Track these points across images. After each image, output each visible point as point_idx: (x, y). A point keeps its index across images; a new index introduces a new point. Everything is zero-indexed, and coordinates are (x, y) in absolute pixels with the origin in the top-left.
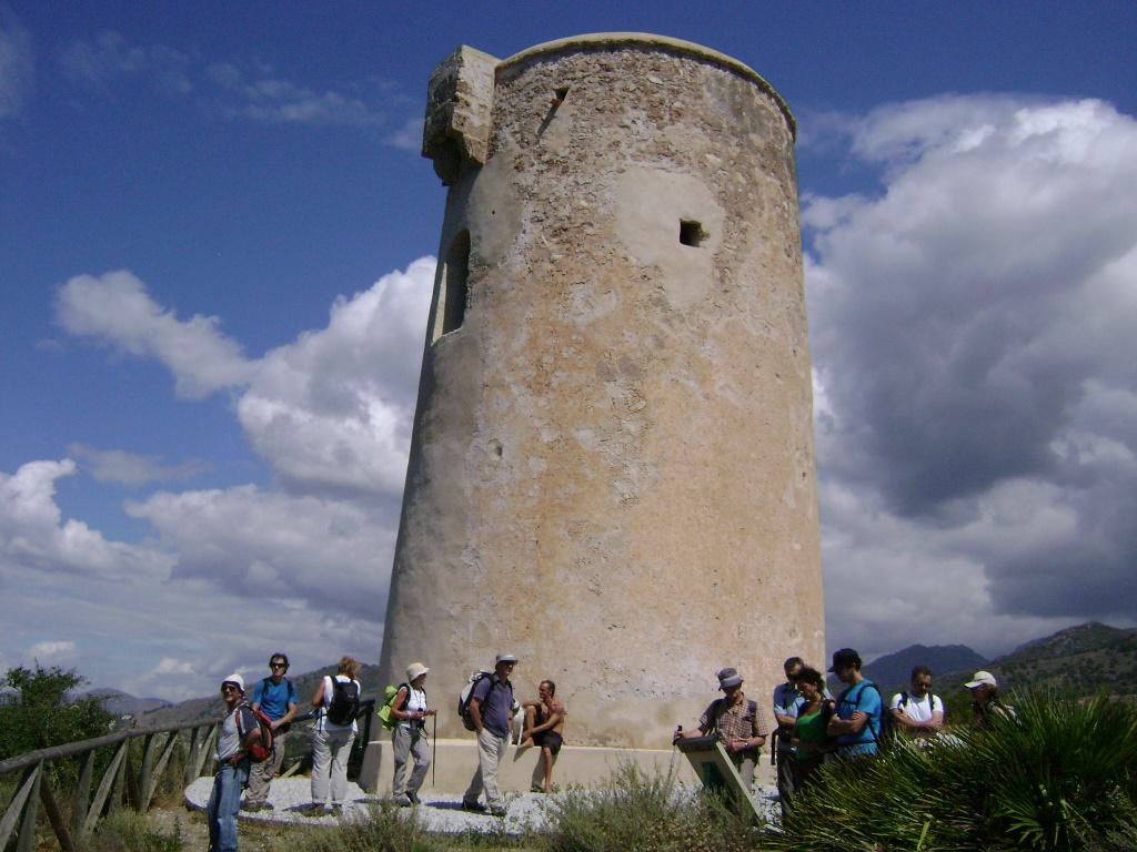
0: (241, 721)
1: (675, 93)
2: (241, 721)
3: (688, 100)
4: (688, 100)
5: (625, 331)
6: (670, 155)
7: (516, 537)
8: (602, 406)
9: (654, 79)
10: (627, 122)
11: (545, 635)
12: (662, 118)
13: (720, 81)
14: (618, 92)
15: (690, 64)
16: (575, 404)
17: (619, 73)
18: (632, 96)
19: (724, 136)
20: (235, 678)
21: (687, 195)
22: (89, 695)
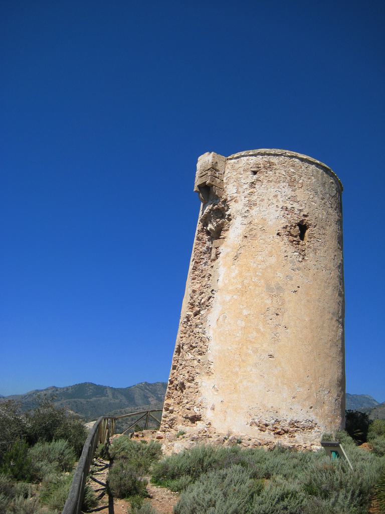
0: (305, 157)
1: (301, 176)
2: (305, 157)
3: (305, 179)
4: (305, 179)
5: (277, 273)
6: (260, 491)
7: (231, 352)
8: (267, 302)
9: (293, 170)
10: (281, 187)
11: (242, 392)
12: (295, 186)
13: (317, 172)
14: (277, 174)
15: (307, 164)
16: (257, 300)
17: (277, 167)
18: (283, 176)
19: (318, 195)
20: (68, 473)
21: (314, 447)
22: (51, 415)
